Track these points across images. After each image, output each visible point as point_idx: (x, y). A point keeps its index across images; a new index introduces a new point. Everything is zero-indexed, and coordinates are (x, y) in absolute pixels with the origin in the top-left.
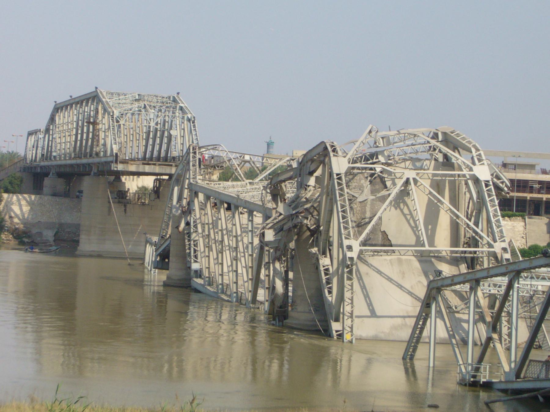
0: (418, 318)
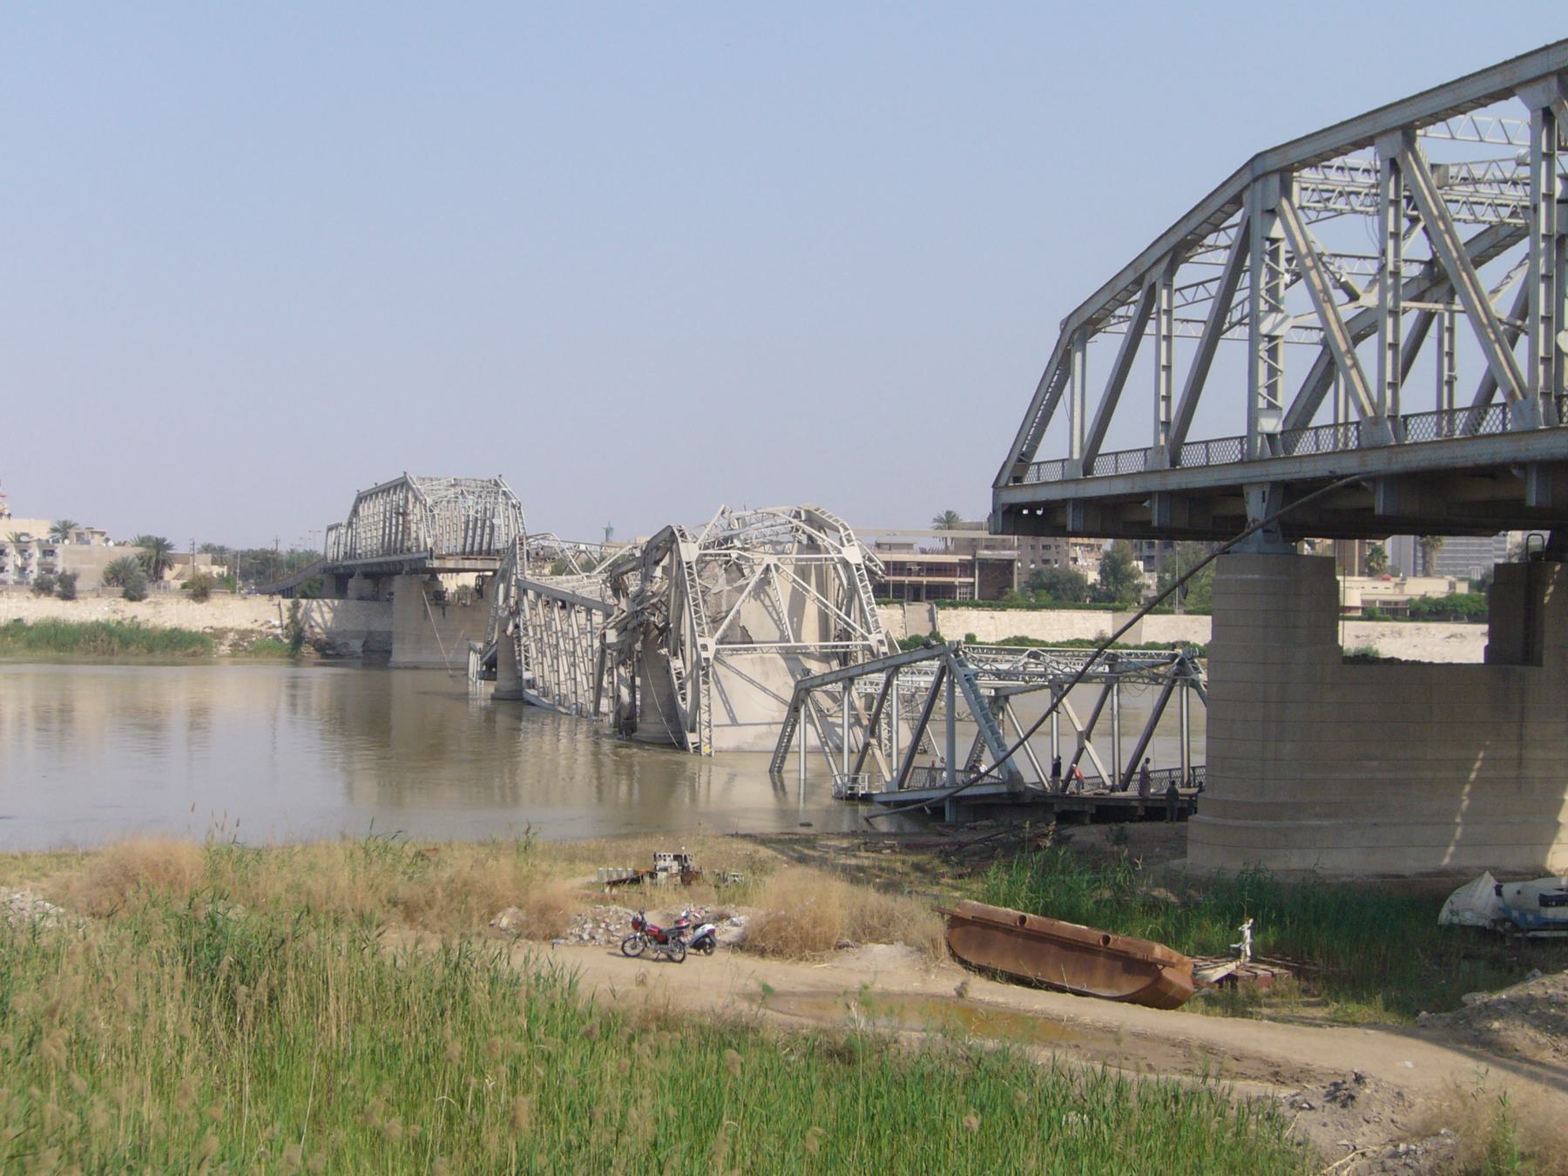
0: (786, 724)
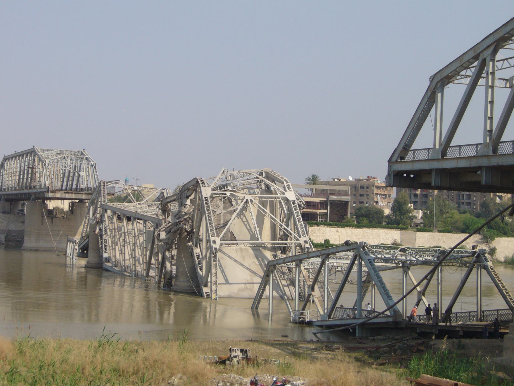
0: (261, 284)
